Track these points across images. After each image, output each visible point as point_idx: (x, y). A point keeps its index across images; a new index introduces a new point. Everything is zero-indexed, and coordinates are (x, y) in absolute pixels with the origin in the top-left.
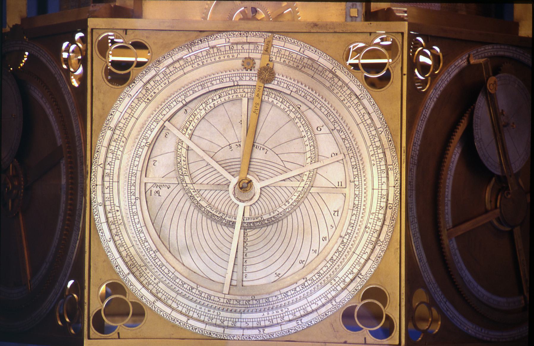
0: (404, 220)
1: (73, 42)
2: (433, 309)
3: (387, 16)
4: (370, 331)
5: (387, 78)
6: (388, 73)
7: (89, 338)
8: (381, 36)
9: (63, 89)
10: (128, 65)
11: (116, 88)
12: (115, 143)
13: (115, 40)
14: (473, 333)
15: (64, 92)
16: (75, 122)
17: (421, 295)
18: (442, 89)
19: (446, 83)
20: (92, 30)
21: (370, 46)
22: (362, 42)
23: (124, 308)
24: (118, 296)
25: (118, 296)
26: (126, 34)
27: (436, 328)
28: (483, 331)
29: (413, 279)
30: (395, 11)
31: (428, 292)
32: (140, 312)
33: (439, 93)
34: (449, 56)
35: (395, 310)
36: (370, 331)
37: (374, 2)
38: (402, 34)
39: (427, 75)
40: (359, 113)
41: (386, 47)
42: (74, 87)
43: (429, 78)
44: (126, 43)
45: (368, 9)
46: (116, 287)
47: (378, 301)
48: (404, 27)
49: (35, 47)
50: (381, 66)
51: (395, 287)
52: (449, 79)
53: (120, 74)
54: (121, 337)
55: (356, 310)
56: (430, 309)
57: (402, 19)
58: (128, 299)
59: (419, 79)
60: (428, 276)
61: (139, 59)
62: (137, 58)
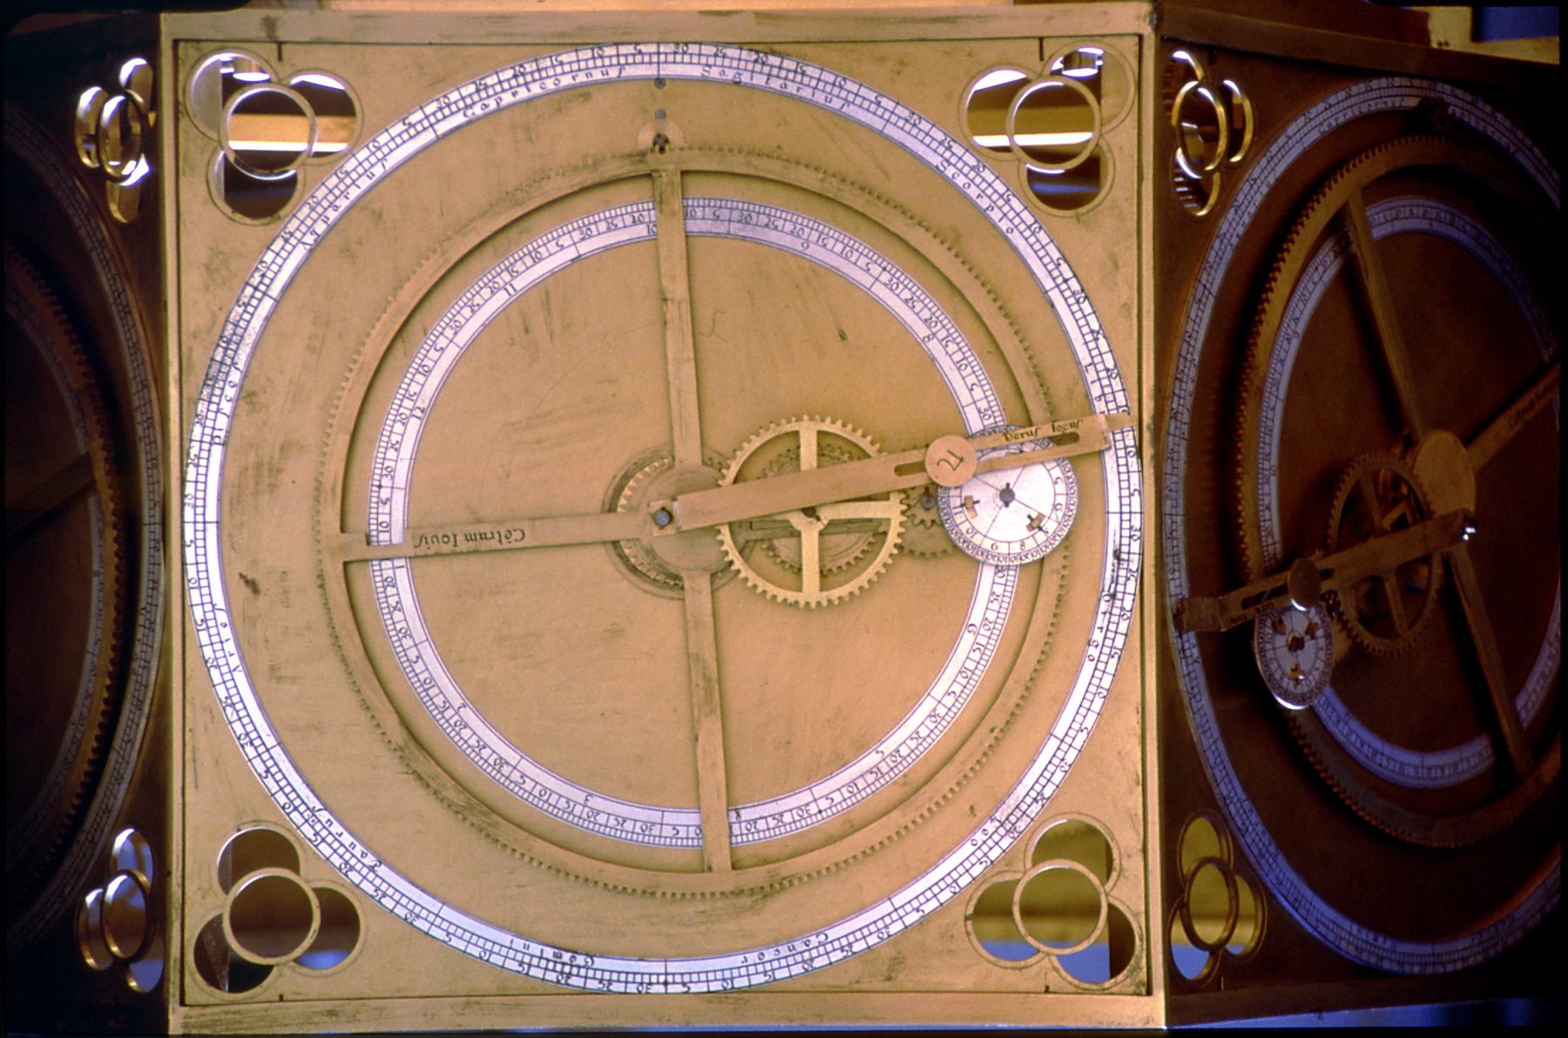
0: (1153, 562)
1: (111, 88)
2: (1238, 878)
7: (182, 1003)
10: (286, 159)
11: (249, 230)
13: (237, 76)
14: (1351, 949)
17: (1201, 837)
18: (1252, 209)
19: (1265, 190)
20: (176, 43)
21: (1041, 77)
23: (286, 914)
26: (280, 58)
27: (1246, 936)
28: (1381, 940)
29: (1183, 793)
31: (1222, 825)
32: (341, 921)
33: (1246, 219)
35: (1135, 890)
37: (167, 1028)
39: (1210, 168)
40: (1042, 253)
42: (116, 222)
43: (1216, 177)
44: (280, 83)
46: (263, 846)
47: (1085, 951)
51: (1131, 812)
53: (257, 190)
54: (1037, 42)
55: (1017, 897)
56: (1230, 882)
58: (308, 880)
59: (1184, 175)
60: (1227, 785)
61: (318, 147)
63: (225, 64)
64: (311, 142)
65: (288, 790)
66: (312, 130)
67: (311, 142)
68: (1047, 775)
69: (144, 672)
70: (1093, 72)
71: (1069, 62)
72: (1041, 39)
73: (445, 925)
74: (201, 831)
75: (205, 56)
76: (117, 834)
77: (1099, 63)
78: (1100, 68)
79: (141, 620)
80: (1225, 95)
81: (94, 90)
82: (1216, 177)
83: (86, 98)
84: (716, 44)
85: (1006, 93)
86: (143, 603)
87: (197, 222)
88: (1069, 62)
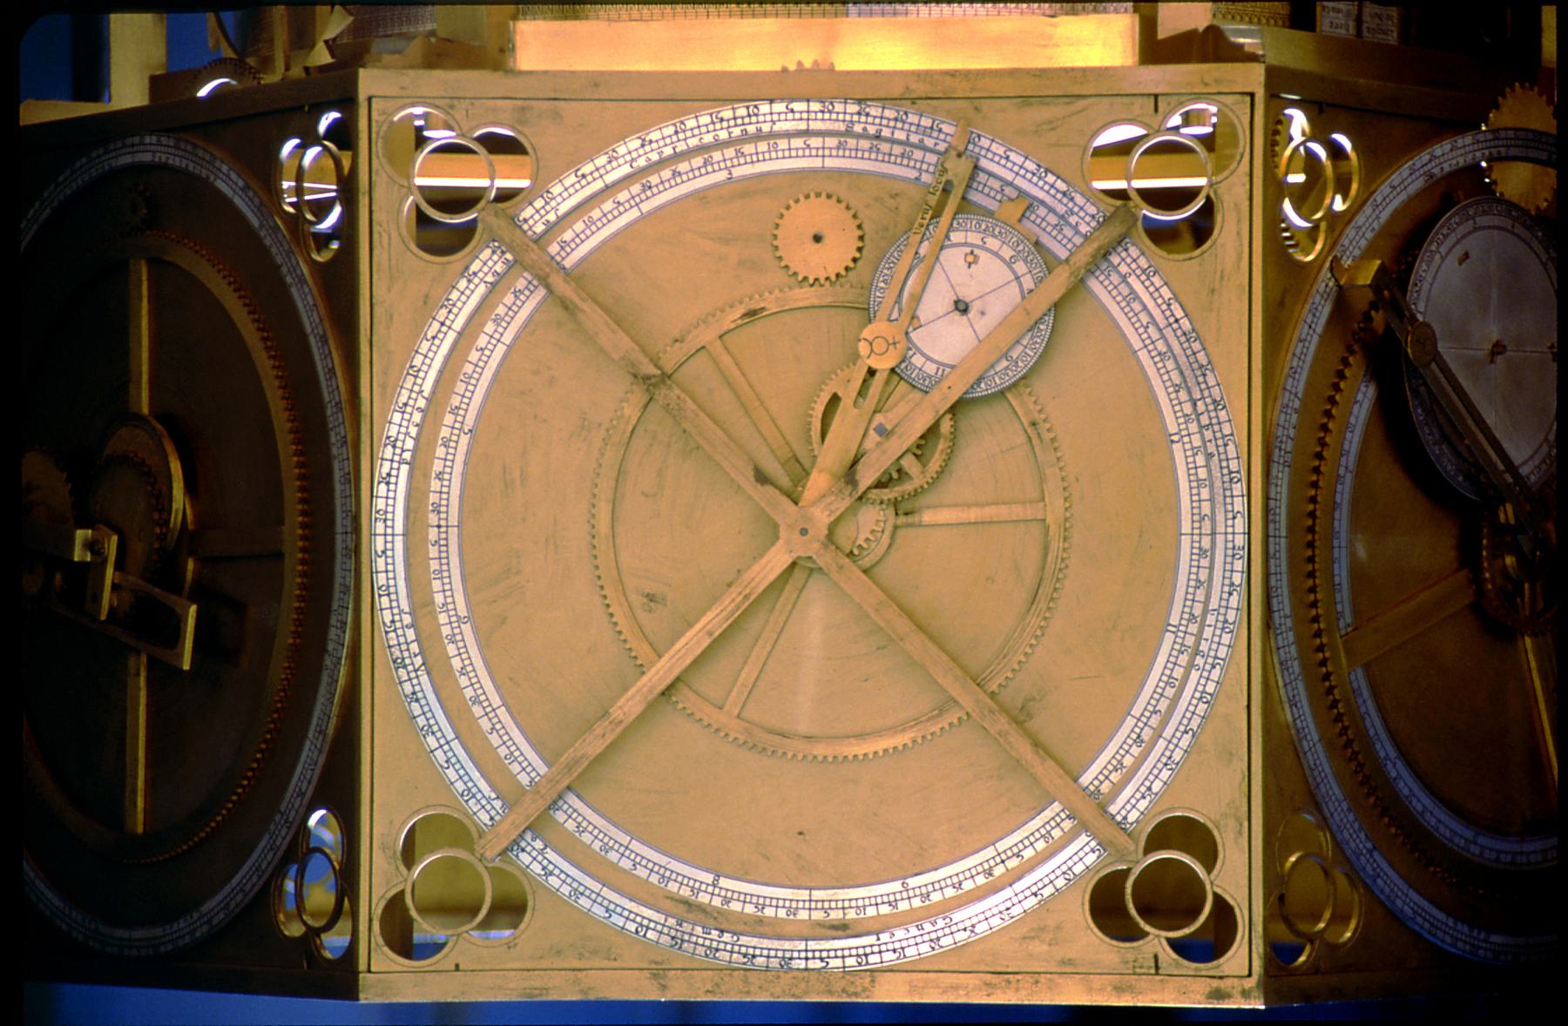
1: (310, 138)
3: (1208, 47)
4: (1169, 940)
5: (1201, 229)
6: (1208, 209)
8: (1205, 103)
9: (284, 270)
12: (452, 417)
15: (289, 279)
16: (325, 357)
20: (370, 99)
21: (1158, 132)
22: (1131, 121)
24: (1186, 859)
25: (1186, 859)
29: (1287, 794)
30: (1228, 34)
34: (1378, 157)
35: (1236, 877)
36: (1169, 940)
38: (1252, 95)
41: (1200, 138)
43: (1323, 225)
45: (1148, 26)
48: (1254, 77)
49: (200, 153)
50: (1187, 195)
52: (1376, 225)
53: (446, 226)
54: (1152, 100)
57: (1253, 58)
61: (501, 183)
62: (1129, 180)
63: (418, 117)
64: (492, 180)
65: (466, 778)
66: (491, 164)
67: (492, 180)
68: (1156, 772)
69: (339, 641)
70: (1210, 130)
71: (1188, 119)
72: (1156, 96)
73: (606, 903)
74: (386, 813)
75: (403, 107)
76: (314, 810)
77: (1214, 120)
78: (1214, 125)
79: (333, 621)
80: (1336, 152)
81: (295, 142)
82: (1323, 225)
83: (290, 145)
84: (859, 101)
85: (1124, 148)
86: (335, 606)
87: (390, 265)
88: (1188, 119)
